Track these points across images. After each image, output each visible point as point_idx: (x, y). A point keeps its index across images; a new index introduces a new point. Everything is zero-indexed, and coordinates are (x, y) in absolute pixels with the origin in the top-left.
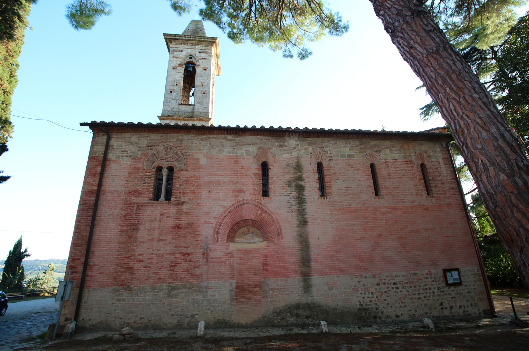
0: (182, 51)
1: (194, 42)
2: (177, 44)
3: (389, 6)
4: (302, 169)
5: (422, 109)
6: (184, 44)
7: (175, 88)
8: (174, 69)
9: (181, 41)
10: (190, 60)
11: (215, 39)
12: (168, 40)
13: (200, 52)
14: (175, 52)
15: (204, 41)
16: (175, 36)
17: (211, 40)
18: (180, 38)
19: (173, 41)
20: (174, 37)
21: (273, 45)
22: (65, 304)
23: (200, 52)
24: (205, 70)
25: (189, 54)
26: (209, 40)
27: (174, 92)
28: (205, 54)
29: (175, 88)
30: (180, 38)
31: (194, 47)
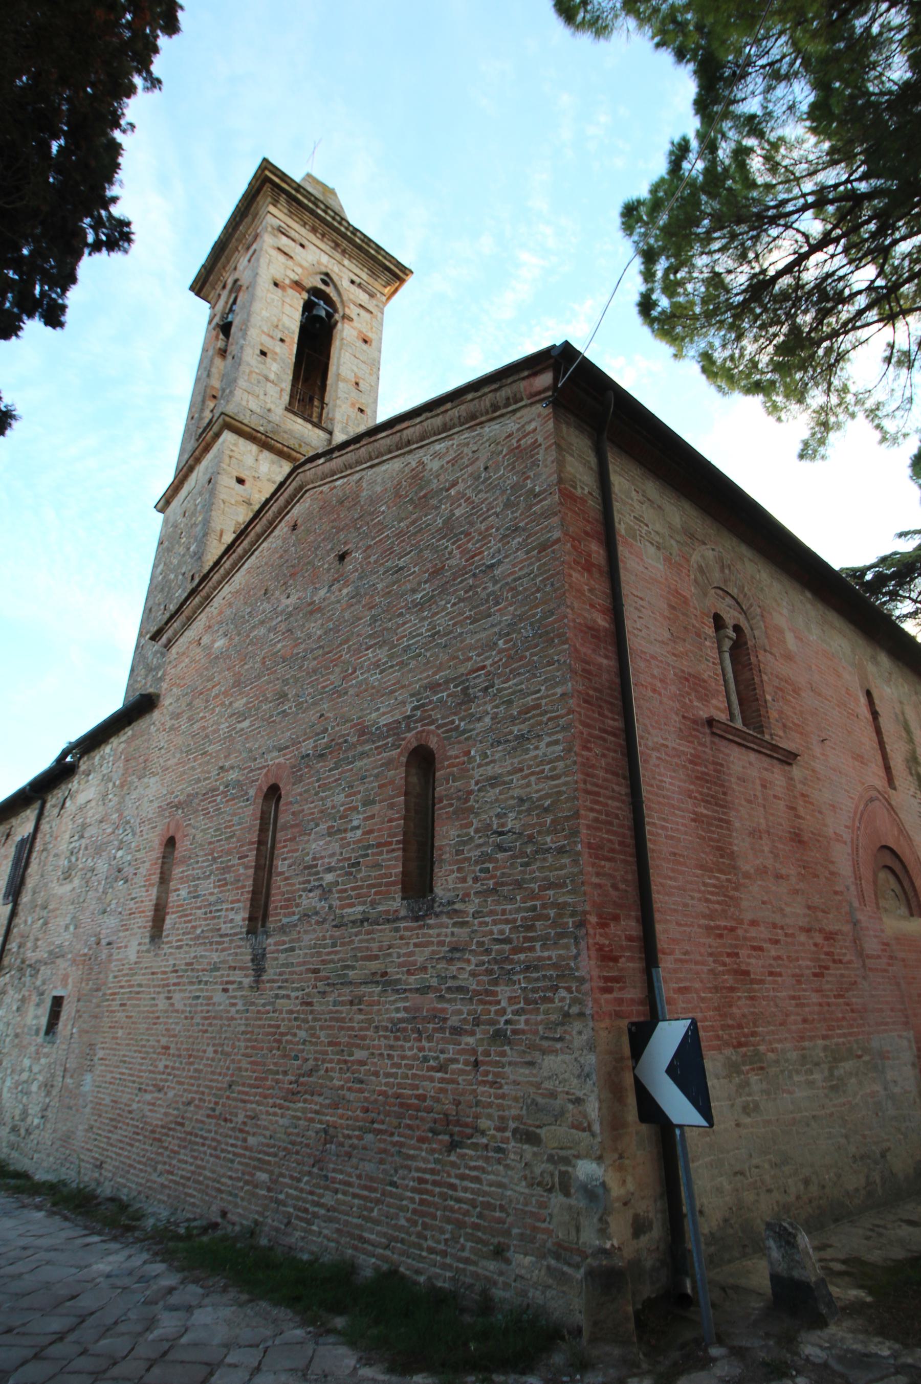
0: (302, 246)
1: (345, 244)
2: (291, 214)
3: (110, 1175)
4: (156, 1254)
5: (774, 409)
6: (314, 230)
7: (278, 348)
8: (276, 285)
9: (307, 216)
10: (323, 287)
11: (406, 271)
12: (267, 187)
13: (353, 282)
14: (284, 238)
15: (373, 258)
16: (297, 191)
17: (392, 267)
18: (311, 205)
19: (283, 199)
20: (293, 192)
21: (240, 334)
22: (836, 382)
23: (353, 282)
24: (365, 342)
25: (324, 270)
26: (387, 263)
27: (274, 360)
28: (367, 296)
29: (278, 350)
30: (311, 205)
31: (338, 256)
